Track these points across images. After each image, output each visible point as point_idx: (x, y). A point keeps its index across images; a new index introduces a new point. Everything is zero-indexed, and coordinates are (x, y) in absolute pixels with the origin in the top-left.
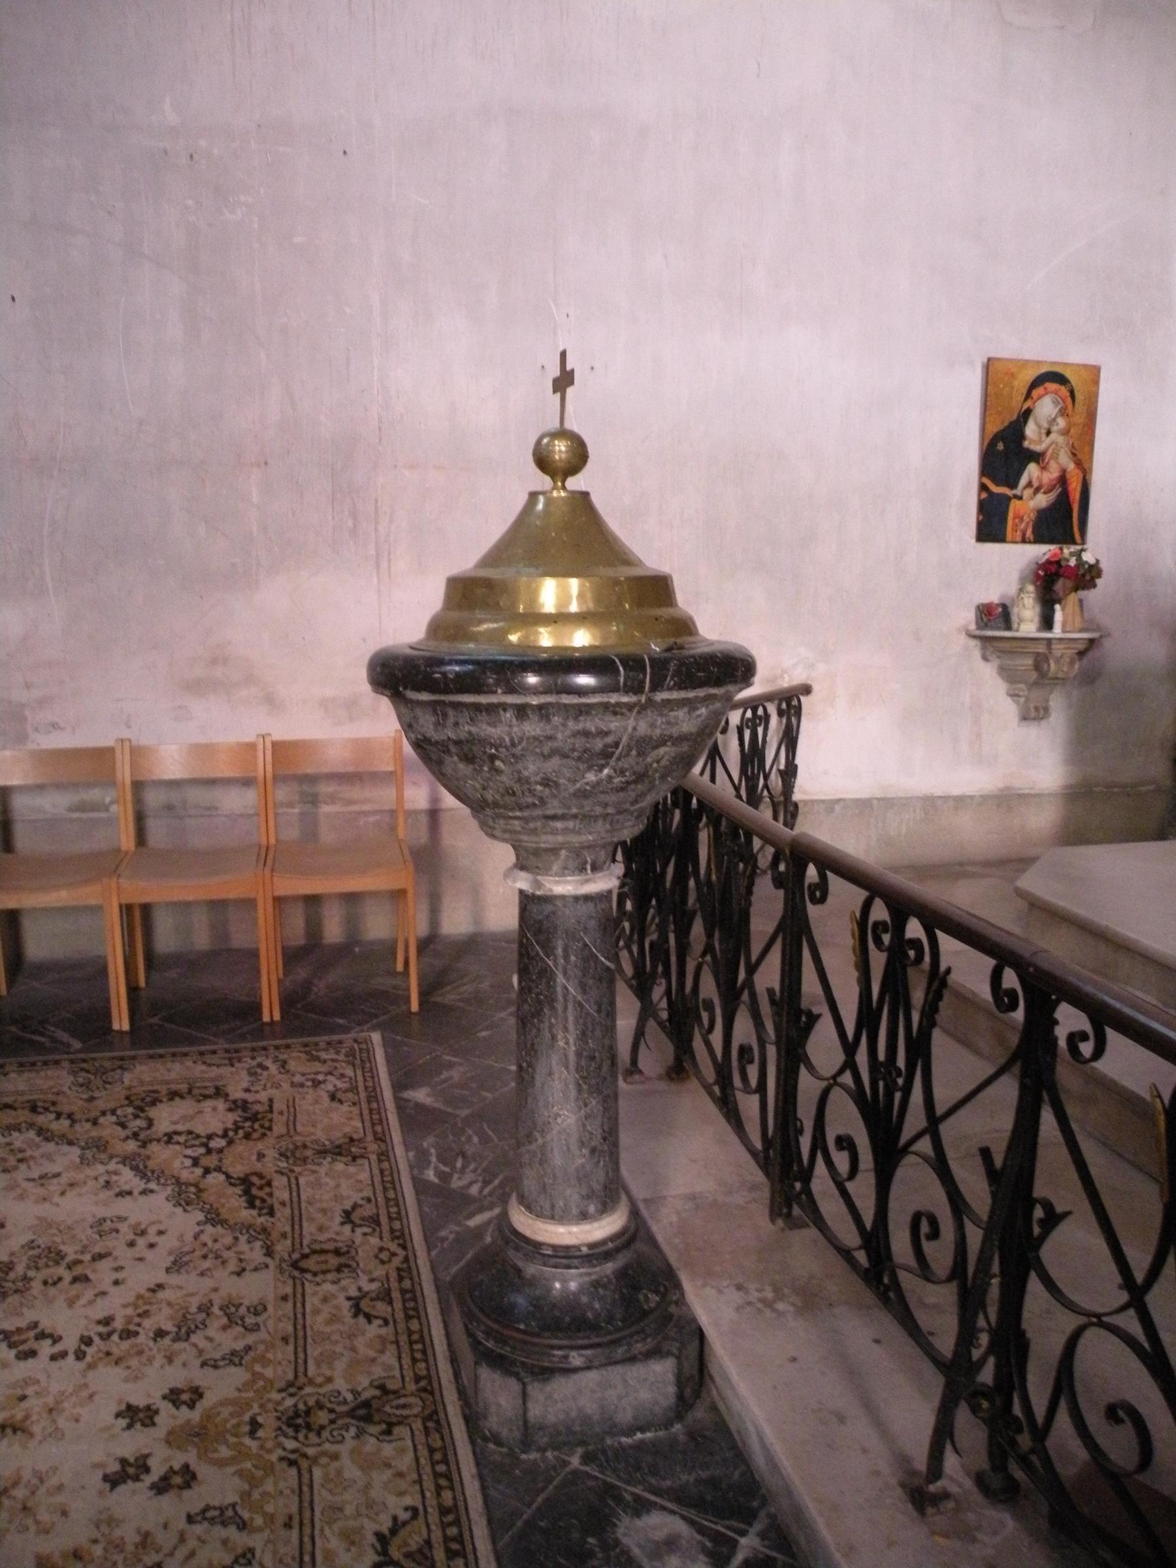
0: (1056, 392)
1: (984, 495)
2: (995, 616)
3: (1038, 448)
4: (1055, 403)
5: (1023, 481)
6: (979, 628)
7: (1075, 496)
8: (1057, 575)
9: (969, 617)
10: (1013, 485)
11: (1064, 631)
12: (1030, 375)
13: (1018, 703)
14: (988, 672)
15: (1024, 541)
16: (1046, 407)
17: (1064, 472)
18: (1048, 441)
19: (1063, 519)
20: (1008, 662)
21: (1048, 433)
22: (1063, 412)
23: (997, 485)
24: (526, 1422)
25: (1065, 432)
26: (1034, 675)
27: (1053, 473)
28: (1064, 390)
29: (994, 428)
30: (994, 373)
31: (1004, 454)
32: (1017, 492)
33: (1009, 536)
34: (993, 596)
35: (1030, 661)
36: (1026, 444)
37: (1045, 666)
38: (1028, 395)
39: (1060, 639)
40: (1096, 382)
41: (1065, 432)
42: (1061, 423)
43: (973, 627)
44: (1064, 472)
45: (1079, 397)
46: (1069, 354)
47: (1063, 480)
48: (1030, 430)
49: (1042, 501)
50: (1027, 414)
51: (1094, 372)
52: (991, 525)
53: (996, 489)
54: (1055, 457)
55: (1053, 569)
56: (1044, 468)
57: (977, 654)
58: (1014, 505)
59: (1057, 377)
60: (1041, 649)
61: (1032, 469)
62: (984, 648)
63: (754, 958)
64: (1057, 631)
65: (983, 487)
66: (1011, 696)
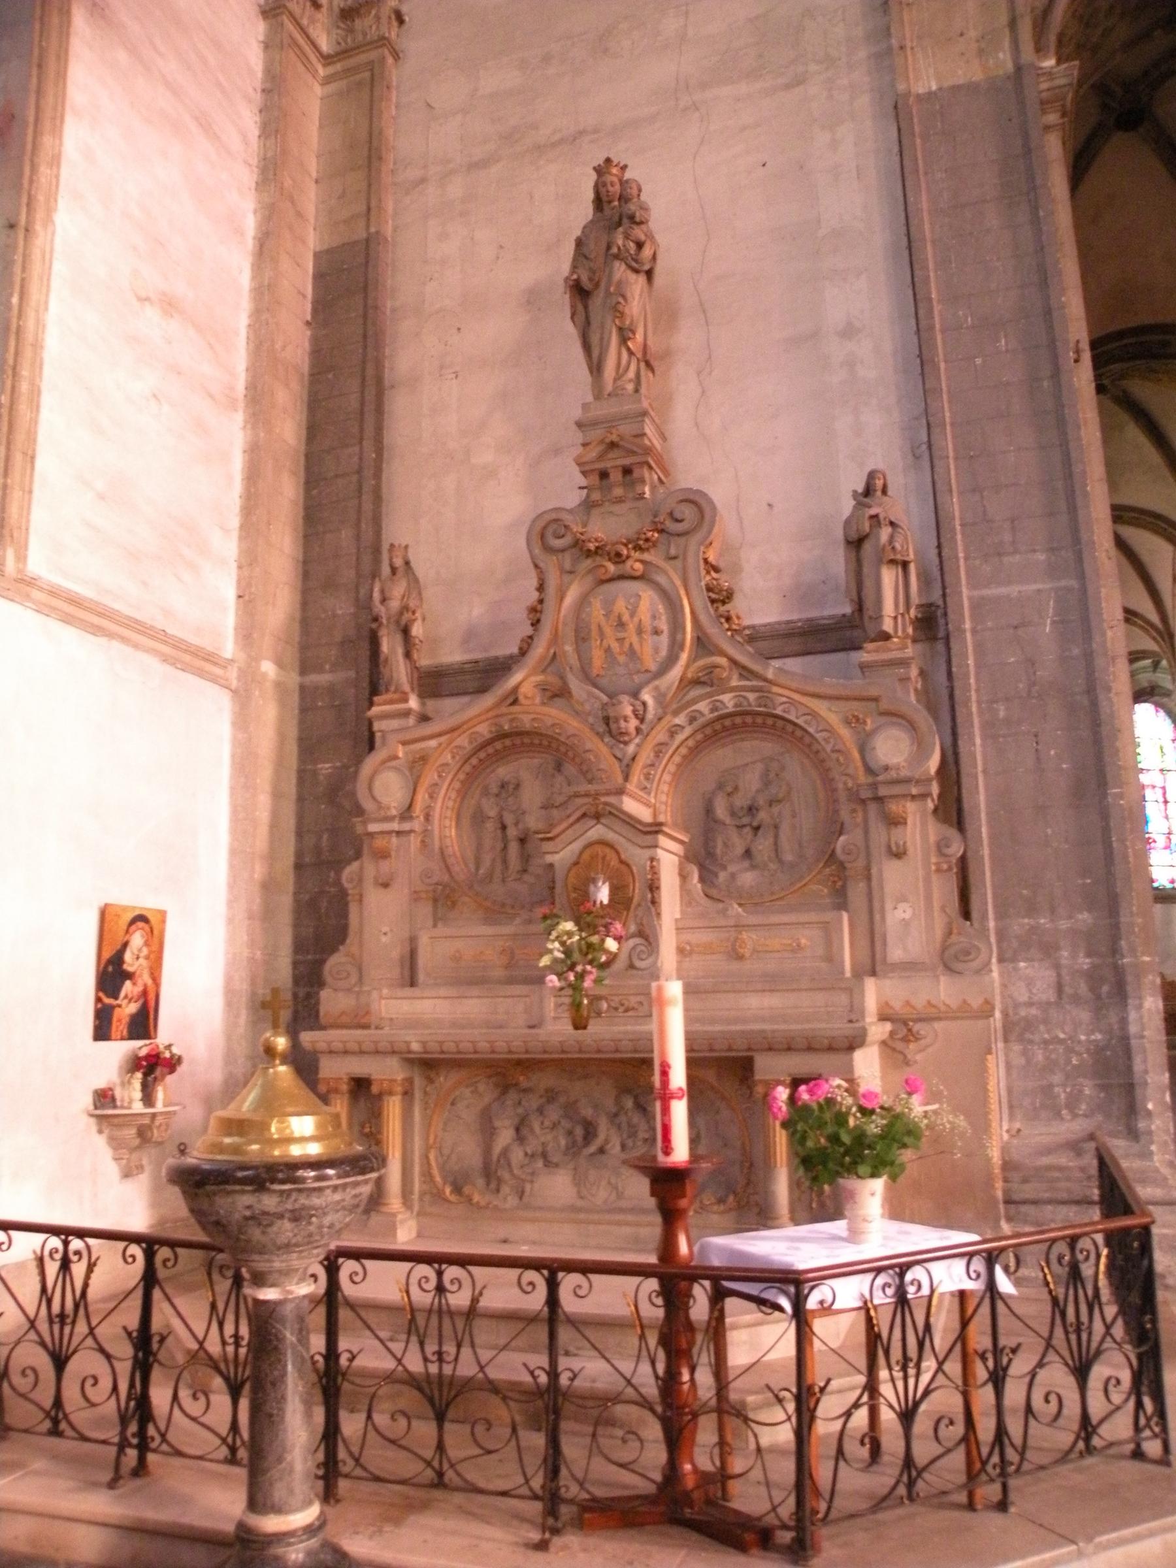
0: (142, 929)
1: (99, 1006)
2: (104, 1097)
3: (130, 969)
4: (143, 936)
5: (122, 994)
6: (96, 1108)
7: (152, 1004)
8: (156, 1064)
9: (88, 1100)
10: (116, 998)
11: (165, 1106)
12: (129, 916)
13: (119, 1165)
14: (100, 1143)
15: (122, 1039)
16: (137, 939)
17: (145, 986)
18: (137, 964)
19: (143, 1024)
20: (118, 1133)
21: (138, 958)
22: (147, 944)
23: (108, 996)
24: (832, 1350)
25: (147, 958)
26: (137, 1141)
27: (139, 989)
28: (146, 927)
29: (107, 955)
30: (105, 914)
31: (112, 975)
32: (118, 1002)
33: (113, 1036)
34: (101, 1084)
35: (133, 1131)
36: (125, 967)
37: (149, 1134)
38: (127, 932)
39: (161, 1113)
40: (164, 921)
41: (147, 958)
42: (145, 951)
43: (91, 1107)
44: (145, 986)
45: (156, 932)
46: (147, 901)
47: (145, 993)
48: (128, 956)
49: (133, 1008)
50: (125, 945)
51: (163, 914)
52: (102, 1032)
53: (107, 1001)
54: (140, 976)
55: (154, 1060)
56: (134, 984)
57: (94, 1128)
58: (117, 1011)
59: (142, 918)
60: (147, 1121)
61: (128, 983)
62: (99, 1124)
63: (221, 1315)
64: (159, 1107)
65: (98, 1000)
66: (116, 1159)
